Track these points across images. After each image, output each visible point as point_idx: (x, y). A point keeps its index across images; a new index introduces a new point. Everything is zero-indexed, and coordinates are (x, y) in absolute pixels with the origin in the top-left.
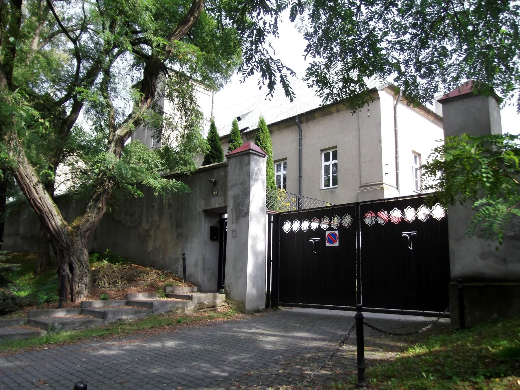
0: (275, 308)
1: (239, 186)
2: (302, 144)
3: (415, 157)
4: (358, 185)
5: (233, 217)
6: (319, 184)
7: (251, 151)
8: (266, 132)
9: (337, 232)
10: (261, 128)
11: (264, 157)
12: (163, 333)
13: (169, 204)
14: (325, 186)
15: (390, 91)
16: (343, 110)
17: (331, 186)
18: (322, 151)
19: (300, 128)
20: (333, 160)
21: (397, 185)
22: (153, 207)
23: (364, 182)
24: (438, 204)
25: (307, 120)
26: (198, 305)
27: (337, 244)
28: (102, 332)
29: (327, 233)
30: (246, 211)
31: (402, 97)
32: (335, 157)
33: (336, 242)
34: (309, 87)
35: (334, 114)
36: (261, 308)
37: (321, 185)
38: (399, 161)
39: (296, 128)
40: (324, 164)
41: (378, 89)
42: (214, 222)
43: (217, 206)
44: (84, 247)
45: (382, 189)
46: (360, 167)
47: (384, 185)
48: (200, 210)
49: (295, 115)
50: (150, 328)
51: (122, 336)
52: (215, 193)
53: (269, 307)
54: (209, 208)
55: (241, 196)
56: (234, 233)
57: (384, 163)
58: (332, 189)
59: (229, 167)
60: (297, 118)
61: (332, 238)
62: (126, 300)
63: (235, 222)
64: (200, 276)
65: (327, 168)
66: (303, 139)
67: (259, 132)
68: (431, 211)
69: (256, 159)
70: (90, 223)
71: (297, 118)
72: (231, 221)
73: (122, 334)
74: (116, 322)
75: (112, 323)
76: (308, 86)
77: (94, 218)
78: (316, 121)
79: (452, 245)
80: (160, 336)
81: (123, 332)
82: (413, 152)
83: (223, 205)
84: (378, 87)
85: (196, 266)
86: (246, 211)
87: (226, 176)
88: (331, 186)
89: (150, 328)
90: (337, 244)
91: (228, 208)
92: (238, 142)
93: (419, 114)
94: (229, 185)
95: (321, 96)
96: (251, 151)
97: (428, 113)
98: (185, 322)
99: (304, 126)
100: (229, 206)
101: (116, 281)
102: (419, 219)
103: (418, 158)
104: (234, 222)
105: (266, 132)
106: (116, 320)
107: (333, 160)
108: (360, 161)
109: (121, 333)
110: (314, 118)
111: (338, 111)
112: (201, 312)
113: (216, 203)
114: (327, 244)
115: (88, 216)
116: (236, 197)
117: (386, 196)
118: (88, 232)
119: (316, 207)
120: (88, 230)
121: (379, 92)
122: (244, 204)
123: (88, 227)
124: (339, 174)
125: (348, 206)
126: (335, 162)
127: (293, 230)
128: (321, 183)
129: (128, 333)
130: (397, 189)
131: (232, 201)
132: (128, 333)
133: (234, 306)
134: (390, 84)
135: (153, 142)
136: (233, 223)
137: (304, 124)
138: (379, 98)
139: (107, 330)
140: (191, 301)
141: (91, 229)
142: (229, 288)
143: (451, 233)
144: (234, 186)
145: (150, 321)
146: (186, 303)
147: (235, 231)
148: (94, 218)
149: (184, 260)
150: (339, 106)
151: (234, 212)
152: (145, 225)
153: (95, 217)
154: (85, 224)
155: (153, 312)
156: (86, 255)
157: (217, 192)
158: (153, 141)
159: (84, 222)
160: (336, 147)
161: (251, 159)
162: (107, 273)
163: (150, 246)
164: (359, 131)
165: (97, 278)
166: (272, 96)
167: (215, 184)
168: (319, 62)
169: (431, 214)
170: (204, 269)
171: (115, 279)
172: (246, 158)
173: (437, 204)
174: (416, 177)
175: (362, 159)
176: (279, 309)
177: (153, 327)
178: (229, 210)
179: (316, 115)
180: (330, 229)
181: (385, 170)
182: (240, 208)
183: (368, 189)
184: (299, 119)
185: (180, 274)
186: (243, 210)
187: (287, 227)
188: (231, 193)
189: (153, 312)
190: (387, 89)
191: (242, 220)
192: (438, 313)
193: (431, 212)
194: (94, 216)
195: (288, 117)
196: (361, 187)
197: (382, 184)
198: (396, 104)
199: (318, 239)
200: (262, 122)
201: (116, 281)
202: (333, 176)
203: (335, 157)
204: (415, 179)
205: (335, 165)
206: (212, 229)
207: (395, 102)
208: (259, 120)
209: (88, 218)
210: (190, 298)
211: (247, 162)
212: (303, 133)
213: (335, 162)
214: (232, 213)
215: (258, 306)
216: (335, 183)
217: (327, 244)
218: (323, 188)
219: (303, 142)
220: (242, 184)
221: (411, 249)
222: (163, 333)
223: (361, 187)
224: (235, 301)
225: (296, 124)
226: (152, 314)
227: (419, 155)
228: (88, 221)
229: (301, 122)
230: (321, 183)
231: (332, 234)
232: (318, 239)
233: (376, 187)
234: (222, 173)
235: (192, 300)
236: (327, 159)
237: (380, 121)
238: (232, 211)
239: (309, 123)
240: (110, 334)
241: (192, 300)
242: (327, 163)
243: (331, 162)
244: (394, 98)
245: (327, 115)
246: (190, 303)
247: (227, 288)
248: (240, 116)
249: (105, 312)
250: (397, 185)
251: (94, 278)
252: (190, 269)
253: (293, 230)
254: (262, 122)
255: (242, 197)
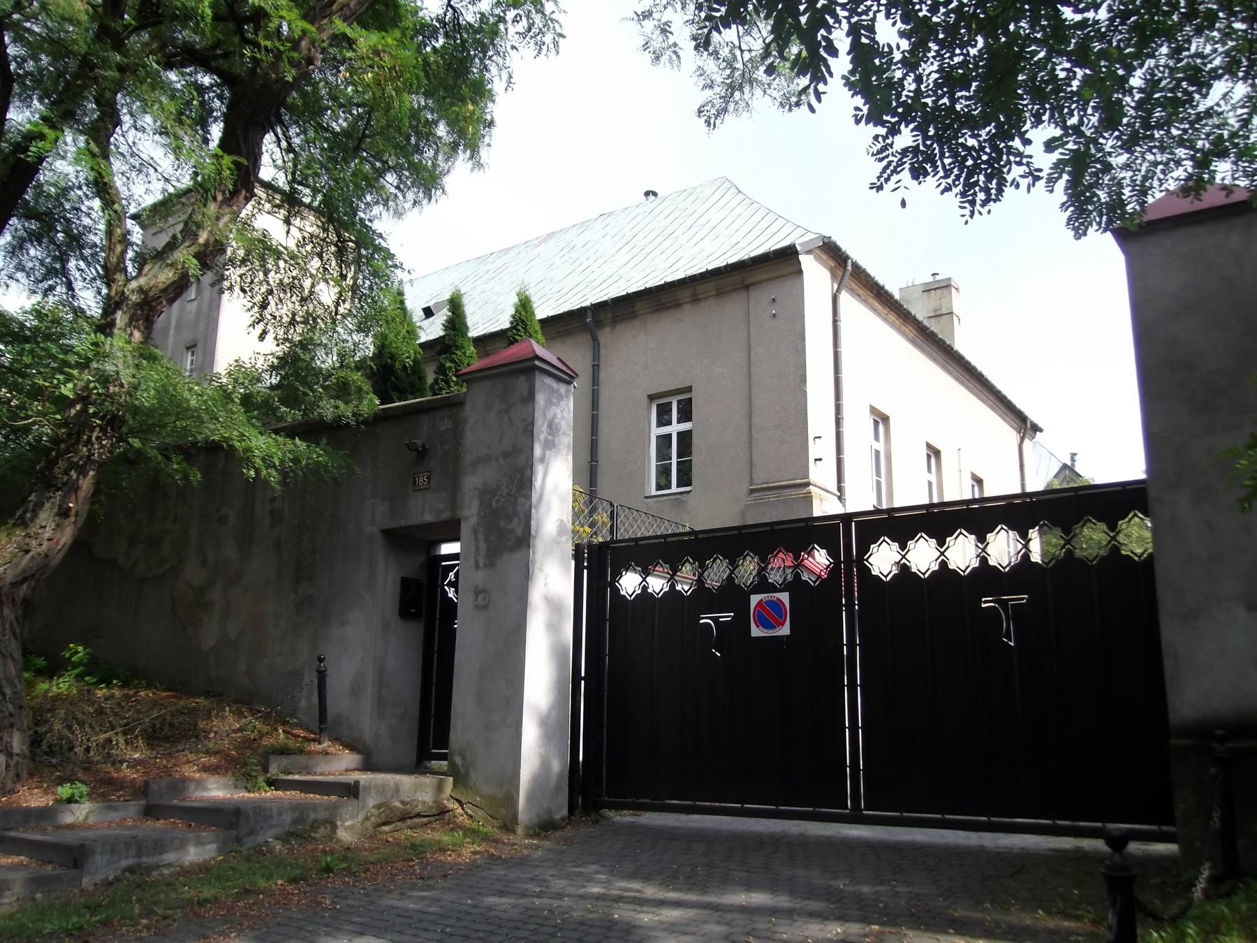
0: (593, 816)
1: (497, 461)
2: (601, 379)
3: (876, 423)
4: (745, 487)
5: (477, 548)
6: (643, 482)
7: (537, 363)
8: (536, 332)
9: (785, 597)
10: (523, 321)
11: (569, 383)
12: (287, 913)
13: (272, 513)
14: (659, 487)
15: (824, 257)
16: (707, 298)
17: (674, 489)
18: (652, 398)
19: (595, 340)
20: (679, 422)
21: (840, 489)
22: (222, 520)
23: (760, 479)
24: (1002, 528)
25: (615, 321)
26: (375, 812)
27: (785, 630)
28: (75, 919)
29: (755, 599)
30: (519, 532)
31: (851, 275)
32: (686, 415)
33: (783, 624)
34: (858, 122)
35: (685, 307)
36: (557, 817)
37: (649, 484)
38: (846, 429)
39: (585, 338)
40: (656, 431)
41: (799, 248)
42: (413, 565)
43: (429, 518)
44: (8, 632)
45: (808, 499)
46: (750, 442)
47: (811, 487)
48: (375, 529)
49: (584, 305)
50: (238, 897)
51: (148, 927)
52: (422, 480)
53: (577, 812)
54: (403, 523)
55: (505, 491)
56: (480, 597)
57: (812, 433)
58: (678, 496)
59: (468, 407)
60: (589, 313)
61: (770, 615)
62: (143, 802)
63: (485, 565)
64: (368, 725)
65: (665, 440)
66: (602, 366)
67: (519, 330)
68: (942, 550)
69: (550, 387)
70: (33, 558)
71: (589, 313)
72: (472, 561)
73: (144, 921)
74: (117, 879)
75: (108, 884)
76: (856, 116)
77: (46, 543)
78: (636, 323)
79: (1171, 633)
80: (278, 924)
81: (148, 913)
82: (873, 410)
83: (445, 516)
84: (800, 244)
85: (355, 691)
86: (519, 531)
87: (457, 433)
88: (674, 489)
89: (238, 897)
90: (785, 630)
91: (463, 524)
92: (464, 353)
93: (885, 320)
94: (468, 458)
95: (881, 156)
96: (537, 363)
97: (904, 321)
98: (344, 869)
99: (605, 335)
100: (467, 518)
101: (109, 740)
102: (950, 567)
103: (881, 427)
104: (481, 563)
105: (536, 332)
106: (119, 872)
107: (679, 422)
108: (750, 426)
109: (141, 916)
110: (634, 316)
111: (696, 300)
112: (386, 833)
113: (423, 510)
114: (756, 632)
115: (28, 536)
116: (487, 493)
117: (817, 513)
118: (25, 587)
119: (651, 533)
120: (24, 580)
121: (802, 258)
122: (516, 514)
123: (24, 571)
124: (697, 459)
125: (781, 527)
126: (685, 426)
127: (650, 590)
128: (649, 480)
129: (165, 918)
130: (840, 498)
131: (475, 504)
132: (165, 918)
133: (480, 813)
134: (826, 240)
135: (192, 361)
136: (477, 566)
137: (607, 330)
138: (800, 272)
139: (93, 909)
140: (354, 801)
141: (33, 576)
142: (464, 758)
143: (1165, 597)
144: (484, 460)
145: (233, 869)
146: (335, 807)
147: (484, 591)
148: (46, 543)
149: (322, 676)
150: (698, 287)
151: (481, 536)
152: (194, 574)
153: (50, 540)
154: (15, 560)
155: (239, 840)
156: (14, 660)
157: (429, 478)
158: (189, 358)
159: (15, 555)
160: (689, 389)
161: (537, 384)
162: (80, 716)
163: (209, 635)
164: (749, 352)
165: (47, 732)
166: (818, 96)
167: (422, 454)
168: (889, 45)
169: (904, 561)
170: (380, 704)
171: (106, 736)
172: (521, 383)
173: (999, 527)
174: (878, 473)
175: (756, 421)
176: (607, 818)
177: (247, 891)
178: (465, 529)
179: (639, 307)
180: (763, 585)
181: (814, 450)
182: (502, 523)
183: (771, 497)
184: (593, 317)
185: (302, 717)
186: (512, 531)
187: (630, 583)
188: (472, 482)
189: (239, 840)
190: (818, 252)
191: (508, 561)
192: (984, 821)
193: (904, 557)
194: (47, 535)
195: (566, 310)
196: (752, 491)
197: (808, 484)
198: (838, 290)
199: (726, 617)
200: (524, 305)
201: (109, 740)
202: (678, 463)
203: (686, 415)
204: (875, 477)
205: (685, 438)
206: (406, 584)
207: (836, 286)
208: (516, 299)
209: (27, 540)
210: (351, 791)
211: (525, 394)
212: (603, 352)
213: (685, 426)
214: (476, 539)
215: (549, 812)
216: (685, 479)
217: (756, 632)
218: (654, 492)
219: (602, 374)
220: (506, 455)
221: (1012, 644)
222: (287, 913)
223: (752, 491)
224: (481, 796)
225: (586, 328)
226: (236, 847)
227: (885, 419)
228: (27, 552)
229: (599, 324)
230: (649, 480)
231: (770, 603)
232: (726, 617)
233: (793, 492)
234: (445, 425)
235: (356, 796)
236: (663, 420)
237: (804, 327)
238: (475, 531)
239: (619, 328)
240: (105, 923)
241: (356, 796)
242: (665, 430)
243: (675, 428)
244: (834, 276)
245: (667, 308)
246: (349, 806)
247: (458, 760)
248: (430, 304)
249: (82, 846)
250: (840, 489)
251: (36, 732)
252: (338, 702)
253: (650, 590)
254: (524, 305)
255: (508, 494)
